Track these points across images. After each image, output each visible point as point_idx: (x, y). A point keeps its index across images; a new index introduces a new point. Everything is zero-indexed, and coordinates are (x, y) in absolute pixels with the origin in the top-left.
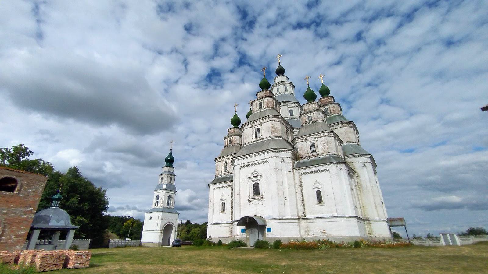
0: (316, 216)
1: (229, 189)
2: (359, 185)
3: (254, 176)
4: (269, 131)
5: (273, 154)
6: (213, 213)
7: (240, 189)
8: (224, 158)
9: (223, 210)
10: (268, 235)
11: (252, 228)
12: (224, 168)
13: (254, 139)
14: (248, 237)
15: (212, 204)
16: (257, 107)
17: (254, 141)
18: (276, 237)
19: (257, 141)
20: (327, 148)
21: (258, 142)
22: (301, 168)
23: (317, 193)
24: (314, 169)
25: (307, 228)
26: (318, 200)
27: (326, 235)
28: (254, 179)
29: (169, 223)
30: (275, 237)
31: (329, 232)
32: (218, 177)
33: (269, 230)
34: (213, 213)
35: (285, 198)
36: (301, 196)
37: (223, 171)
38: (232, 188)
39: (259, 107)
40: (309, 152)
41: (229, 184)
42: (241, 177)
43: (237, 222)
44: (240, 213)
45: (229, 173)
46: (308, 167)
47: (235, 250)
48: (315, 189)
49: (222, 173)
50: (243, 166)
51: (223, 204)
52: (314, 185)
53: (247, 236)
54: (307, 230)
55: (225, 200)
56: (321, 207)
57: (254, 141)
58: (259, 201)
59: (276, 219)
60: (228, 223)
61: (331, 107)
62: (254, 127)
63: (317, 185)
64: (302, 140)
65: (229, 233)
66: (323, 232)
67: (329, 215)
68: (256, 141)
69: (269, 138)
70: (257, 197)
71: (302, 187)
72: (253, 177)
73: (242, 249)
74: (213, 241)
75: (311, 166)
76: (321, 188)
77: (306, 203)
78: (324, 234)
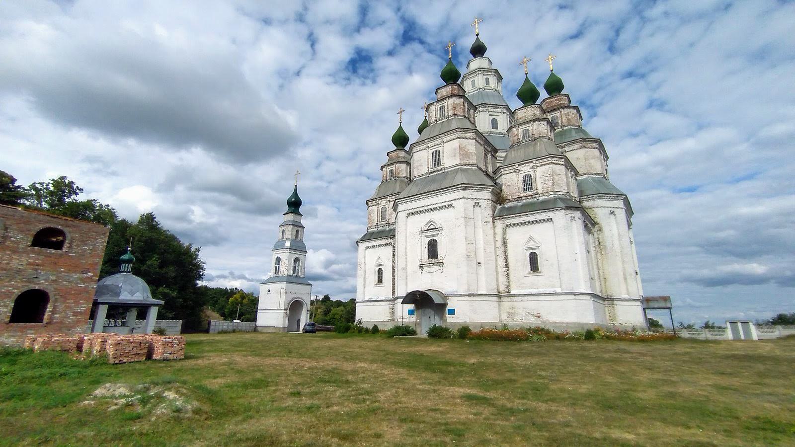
5: (461, 193)
6: (365, 284)
9: (380, 281)
13: (430, 169)
14: (418, 321)
16: (436, 115)
18: (462, 322)
19: (436, 171)
20: (551, 184)
23: (530, 255)
28: (428, 233)
30: (461, 321)
32: (372, 230)
33: (452, 312)
34: (365, 284)
38: (394, 247)
40: (521, 190)
41: (390, 241)
51: (380, 272)
55: (383, 265)
56: (536, 278)
63: (531, 244)
70: (433, 261)
72: (428, 230)
74: (364, 326)
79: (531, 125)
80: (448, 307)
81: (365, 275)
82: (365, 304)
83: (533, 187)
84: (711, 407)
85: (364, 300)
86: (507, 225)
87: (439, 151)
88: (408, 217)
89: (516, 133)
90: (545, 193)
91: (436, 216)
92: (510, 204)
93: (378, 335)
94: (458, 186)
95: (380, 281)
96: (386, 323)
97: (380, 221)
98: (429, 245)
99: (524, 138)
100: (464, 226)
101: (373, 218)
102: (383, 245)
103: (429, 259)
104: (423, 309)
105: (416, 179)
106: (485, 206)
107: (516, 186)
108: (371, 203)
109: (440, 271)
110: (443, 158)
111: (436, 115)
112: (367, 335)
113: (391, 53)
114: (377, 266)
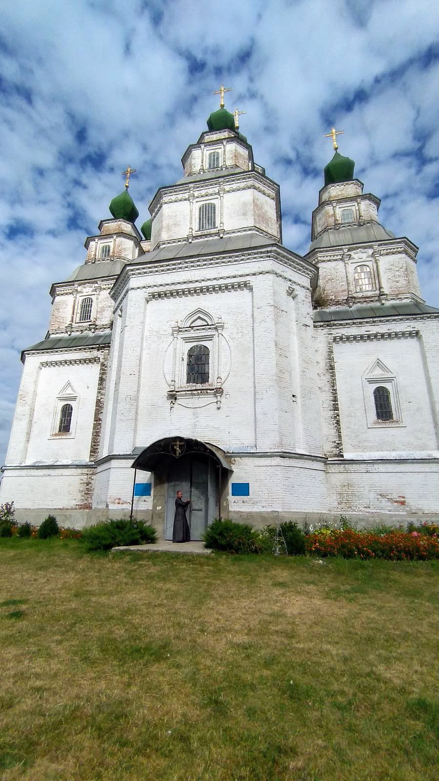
0: (377, 455)
1: (96, 369)
4: (245, 214)
5: (268, 264)
6: (29, 434)
7: (140, 360)
8: (85, 284)
9: (65, 427)
10: (236, 506)
11: (176, 480)
12: (79, 311)
13: (194, 232)
14: (159, 508)
15: (27, 409)
16: (202, 162)
17: (196, 237)
18: (267, 513)
19: (206, 236)
20: (405, 282)
21: (206, 239)
22: (336, 322)
23: (375, 393)
24: (374, 329)
25: (346, 488)
26: (377, 413)
27: (407, 511)
28: (192, 334)
30: (263, 510)
31: (414, 503)
32: (58, 335)
33: (242, 490)
34: (29, 434)
35: (293, 396)
36: (332, 398)
37: (77, 318)
38: (103, 365)
41: (96, 353)
42: (147, 324)
43: (134, 460)
44: (135, 431)
45: (94, 327)
46: (358, 321)
47: (127, 558)
48: (371, 381)
51: (67, 412)
52: (372, 370)
53: (155, 506)
54: (346, 495)
55: (74, 399)
56: (387, 432)
57: (196, 237)
59: (268, 456)
60: (78, 466)
62: (198, 200)
63: (378, 373)
64: (335, 258)
65: (79, 496)
66: (396, 502)
67: (418, 455)
68: (201, 236)
69: (239, 234)
71: (333, 375)
73: (131, 553)
74: (20, 519)
75: (368, 320)
76: (389, 380)
77: (342, 418)
78: (402, 507)
80: (234, 479)
81: (32, 415)
82: (24, 472)
84: (147, 560)
86: (335, 339)
87: (213, 207)
88: (148, 302)
89: (331, 212)
90: (397, 296)
91: (209, 303)
92: (333, 308)
93: (58, 542)
94: (263, 250)
95: (65, 427)
96: (68, 513)
97: (78, 320)
98: (190, 356)
100: (274, 322)
101: (61, 314)
104: (172, 484)
105: (164, 246)
107: (343, 281)
108: (62, 289)
109: (215, 406)
111: (202, 162)
112: (26, 541)
113: (53, 233)
114: (61, 399)
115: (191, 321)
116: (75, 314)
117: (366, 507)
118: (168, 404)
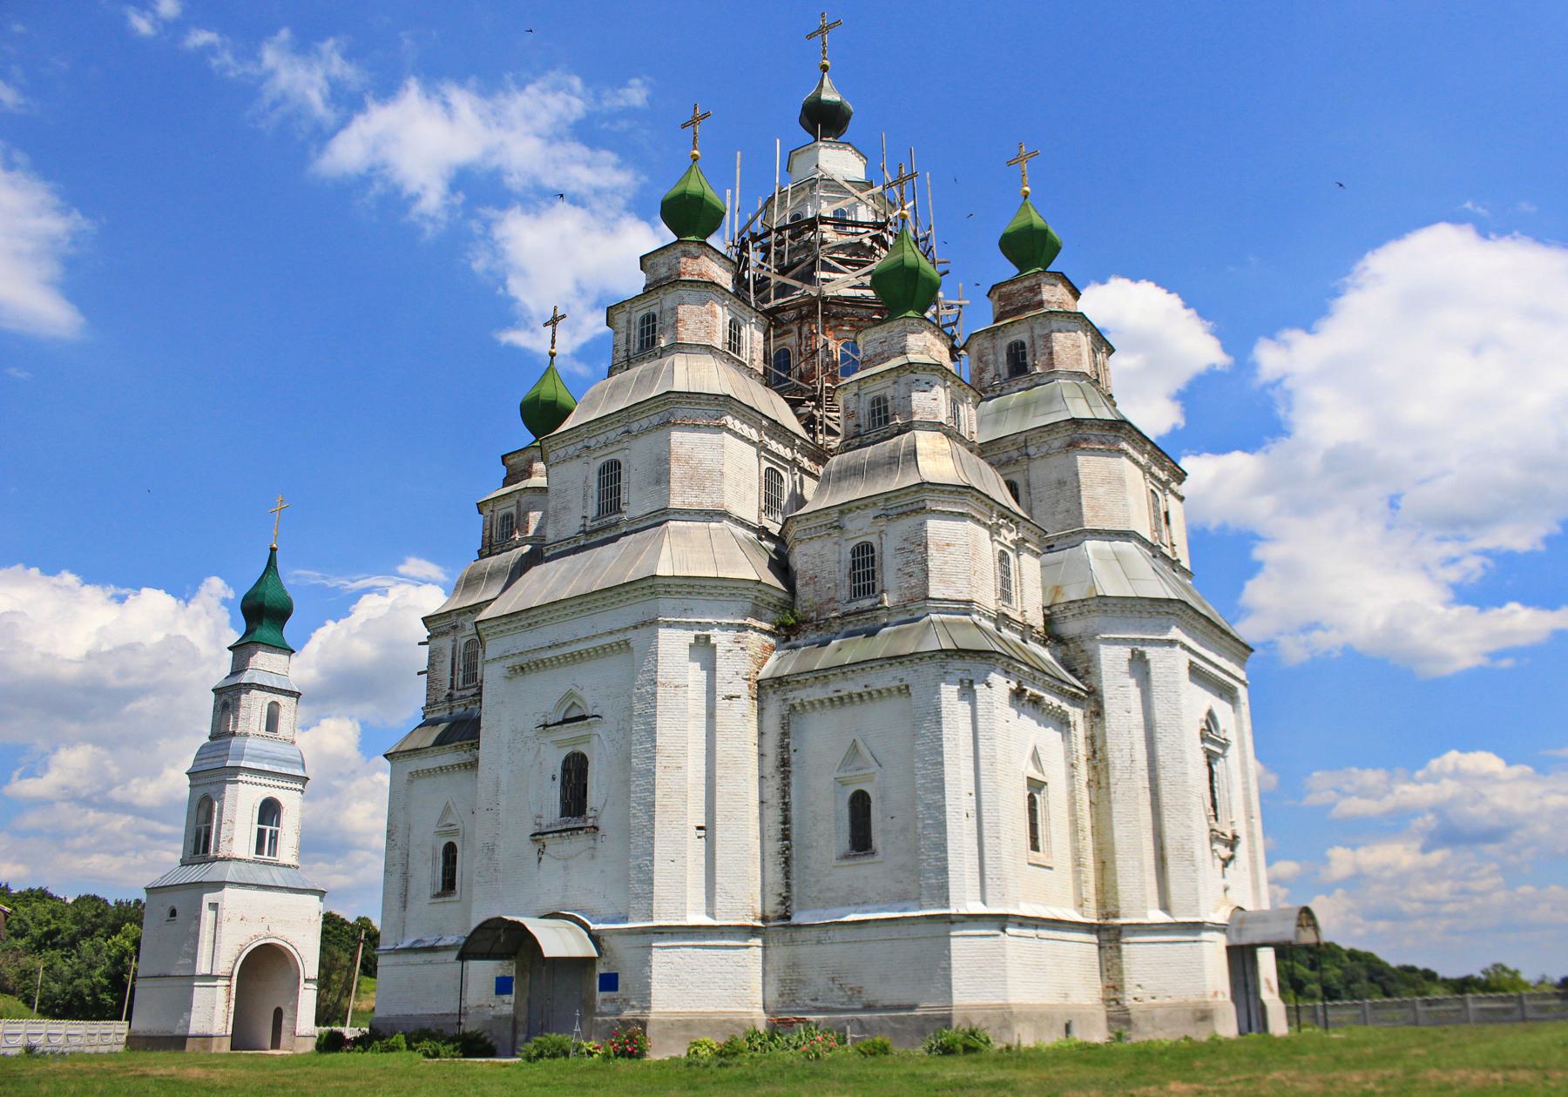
2: (1098, 755)
3: (569, 716)
12: (461, 667)
29: (268, 941)
39: (642, 342)
40: (845, 593)
49: (450, 695)
50: (522, 668)
56: (864, 871)
58: (580, 842)
61: (1040, 336)
68: (596, 531)
70: (574, 823)
71: (786, 776)
72: (565, 721)
79: (657, 301)
82: (401, 958)
83: (877, 584)
85: (400, 946)
97: (460, 686)
99: (874, 426)
102: (458, 765)
103: (562, 816)
106: (729, 646)
110: (586, 486)
115: (563, 711)
116: (456, 672)
117: (812, 1000)
118: (531, 850)
